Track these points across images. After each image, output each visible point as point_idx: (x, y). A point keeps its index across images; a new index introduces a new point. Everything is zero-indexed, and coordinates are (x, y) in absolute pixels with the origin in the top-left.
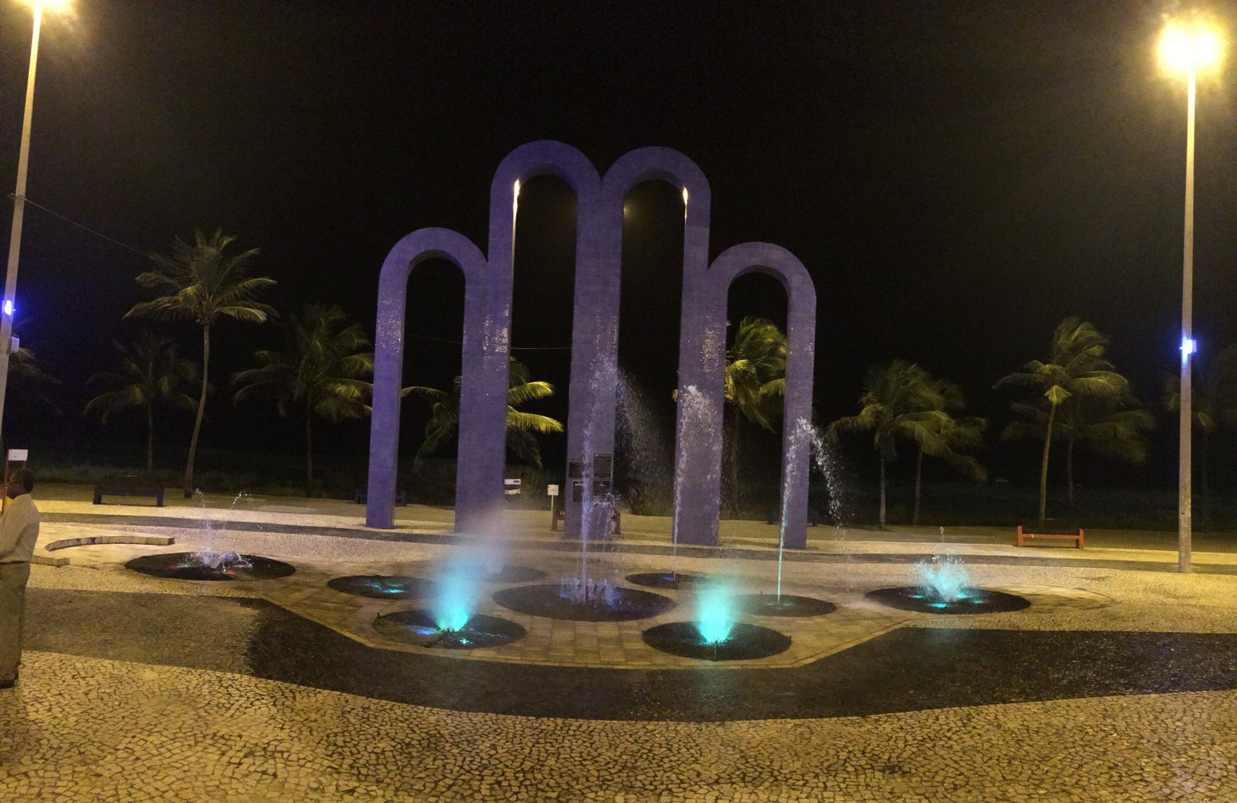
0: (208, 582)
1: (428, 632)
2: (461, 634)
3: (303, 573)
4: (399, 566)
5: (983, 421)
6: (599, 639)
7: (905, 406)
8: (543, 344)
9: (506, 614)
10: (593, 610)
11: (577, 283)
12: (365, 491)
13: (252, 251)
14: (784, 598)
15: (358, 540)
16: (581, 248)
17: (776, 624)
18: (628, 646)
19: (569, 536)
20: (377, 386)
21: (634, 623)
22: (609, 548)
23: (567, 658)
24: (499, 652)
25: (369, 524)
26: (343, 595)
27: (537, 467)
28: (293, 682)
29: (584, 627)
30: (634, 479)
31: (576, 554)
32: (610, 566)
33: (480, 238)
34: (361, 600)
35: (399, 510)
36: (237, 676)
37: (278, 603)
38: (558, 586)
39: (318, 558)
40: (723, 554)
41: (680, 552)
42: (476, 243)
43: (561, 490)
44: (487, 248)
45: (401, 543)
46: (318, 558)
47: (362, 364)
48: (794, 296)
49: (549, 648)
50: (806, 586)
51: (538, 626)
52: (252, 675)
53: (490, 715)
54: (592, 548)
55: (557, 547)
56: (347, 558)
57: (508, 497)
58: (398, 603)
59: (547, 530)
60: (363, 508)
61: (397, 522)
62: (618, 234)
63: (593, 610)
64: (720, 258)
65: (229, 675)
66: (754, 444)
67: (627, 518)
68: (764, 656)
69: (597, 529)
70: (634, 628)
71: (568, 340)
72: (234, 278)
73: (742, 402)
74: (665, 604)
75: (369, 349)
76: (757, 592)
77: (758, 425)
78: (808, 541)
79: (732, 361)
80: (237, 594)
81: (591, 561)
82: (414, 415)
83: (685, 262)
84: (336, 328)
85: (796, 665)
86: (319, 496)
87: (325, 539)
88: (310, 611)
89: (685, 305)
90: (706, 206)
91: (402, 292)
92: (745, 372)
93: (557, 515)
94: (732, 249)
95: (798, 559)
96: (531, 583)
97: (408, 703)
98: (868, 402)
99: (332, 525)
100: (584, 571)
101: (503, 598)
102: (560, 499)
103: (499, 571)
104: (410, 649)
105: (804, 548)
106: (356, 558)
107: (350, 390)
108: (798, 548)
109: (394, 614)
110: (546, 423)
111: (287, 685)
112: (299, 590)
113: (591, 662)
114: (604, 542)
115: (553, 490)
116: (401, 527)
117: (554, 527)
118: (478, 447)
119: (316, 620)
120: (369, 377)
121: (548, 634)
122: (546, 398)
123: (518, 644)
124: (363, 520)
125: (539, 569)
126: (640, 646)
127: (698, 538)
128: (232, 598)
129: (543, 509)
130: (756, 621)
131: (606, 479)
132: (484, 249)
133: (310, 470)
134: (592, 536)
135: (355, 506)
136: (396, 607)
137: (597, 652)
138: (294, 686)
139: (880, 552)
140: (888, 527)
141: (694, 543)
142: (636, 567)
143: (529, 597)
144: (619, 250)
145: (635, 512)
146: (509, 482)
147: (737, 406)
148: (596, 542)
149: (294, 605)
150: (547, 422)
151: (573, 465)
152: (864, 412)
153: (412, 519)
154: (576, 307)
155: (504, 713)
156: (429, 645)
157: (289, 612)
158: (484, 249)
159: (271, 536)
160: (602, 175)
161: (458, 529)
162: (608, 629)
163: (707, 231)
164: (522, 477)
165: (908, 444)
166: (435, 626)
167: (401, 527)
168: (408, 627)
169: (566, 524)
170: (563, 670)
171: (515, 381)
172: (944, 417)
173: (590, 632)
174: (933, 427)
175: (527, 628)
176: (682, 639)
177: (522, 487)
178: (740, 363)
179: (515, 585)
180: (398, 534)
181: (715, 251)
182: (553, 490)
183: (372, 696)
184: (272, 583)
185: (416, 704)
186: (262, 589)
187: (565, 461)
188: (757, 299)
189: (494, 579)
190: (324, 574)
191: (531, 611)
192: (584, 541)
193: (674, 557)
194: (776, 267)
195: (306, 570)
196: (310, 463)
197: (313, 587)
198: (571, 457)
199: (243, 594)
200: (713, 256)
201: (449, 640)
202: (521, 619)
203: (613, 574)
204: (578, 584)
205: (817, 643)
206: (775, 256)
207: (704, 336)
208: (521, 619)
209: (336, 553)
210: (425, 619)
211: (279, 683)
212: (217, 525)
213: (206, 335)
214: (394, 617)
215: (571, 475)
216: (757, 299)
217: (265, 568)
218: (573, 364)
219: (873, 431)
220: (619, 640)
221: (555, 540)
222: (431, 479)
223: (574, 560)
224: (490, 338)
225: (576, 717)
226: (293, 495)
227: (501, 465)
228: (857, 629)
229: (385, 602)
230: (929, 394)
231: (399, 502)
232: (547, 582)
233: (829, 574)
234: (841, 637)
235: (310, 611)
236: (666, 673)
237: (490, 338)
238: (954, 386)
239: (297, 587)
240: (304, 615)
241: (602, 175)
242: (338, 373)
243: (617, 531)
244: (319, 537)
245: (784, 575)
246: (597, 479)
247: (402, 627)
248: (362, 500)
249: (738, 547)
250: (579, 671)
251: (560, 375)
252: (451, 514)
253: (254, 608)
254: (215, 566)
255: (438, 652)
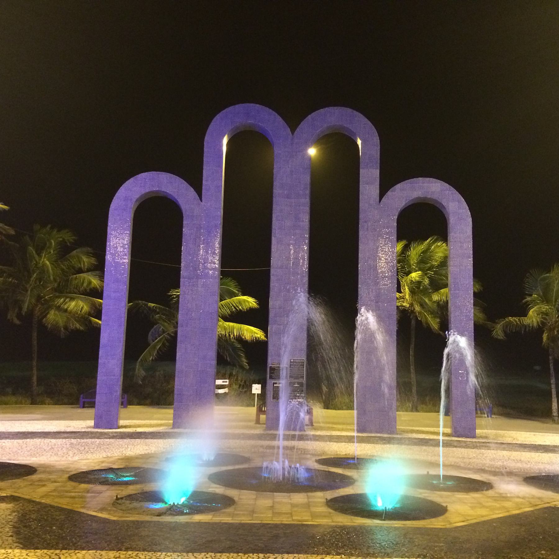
1: (159, 506)
3: (44, 472)
4: (128, 459)
6: (293, 506)
9: (219, 490)
10: (290, 485)
11: (274, 219)
12: (93, 395)
14: (446, 477)
15: (89, 441)
16: (277, 191)
17: (437, 497)
18: (314, 509)
19: (269, 428)
20: (106, 303)
21: (319, 494)
22: (301, 438)
23: (268, 518)
25: (96, 426)
26: (83, 486)
28: (56, 549)
30: (323, 380)
32: (304, 452)
33: (196, 183)
35: (123, 412)
36: (10, 551)
37: (27, 497)
39: (56, 458)
40: (400, 442)
41: (361, 440)
42: (191, 185)
43: (263, 388)
44: (201, 194)
46: (56, 458)
48: (452, 220)
50: (469, 469)
51: (245, 497)
52: (22, 549)
53: (210, 554)
54: (287, 438)
55: (260, 437)
57: (218, 395)
58: (131, 487)
59: (252, 424)
60: (91, 412)
62: (307, 179)
63: (290, 485)
64: (389, 193)
67: (319, 412)
68: (424, 519)
69: (293, 422)
70: (320, 497)
71: (268, 264)
73: (417, 308)
74: (346, 481)
75: (99, 267)
76: (423, 472)
78: (478, 431)
81: (286, 448)
82: (138, 330)
83: (361, 197)
84: (65, 251)
86: (43, 403)
87: (59, 441)
88: (56, 500)
91: (129, 224)
92: (419, 283)
93: (260, 411)
94: (398, 186)
95: (467, 446)
96: (237, 467)
97: (149, 551)
98: (534, 302)
99: (62, 429)
101: (217, 478)
102: (262, 396)
103: (212, 458)
104: (147, 518)
105: (474, 437)
106: (89, 456)
107: (78, 305)
109: (129, 496)
110: (251, 332)
111: (52, 551)
112: (44, 485)
113: (286, 520)
114: (297, 433)
115: (256, 389)
116: (125, 427)
117: (258, 421)
118: (194, 356)
120: (98, 293)
121: (252, 502)
122: (251, 310)
124: (91, 423)
125: (246, 455)
126: (324, 509)
127: (376, 426)
129: (248, 406)
130: (421, 493)
131: (300, 380)
132: (199, 190)
133: (35, 379)
134: (288, 427)
135: (80, 410)
136: (131, 490)
138: (58, 551)
141: (377, 432)
142: (324, 453)
143: (240, 474)
145: (327, 407)
146: (219, 382)
147: (413, 312)
149: (42, 497)
150: (252, 332)
151: (272, 369)
152: (531, 313)
153: (136, 419)
154: (273, 238)
155: (220, 552)
156: (159, 515)
157: (39, 503)
158: (199, 190)
162: (299, 498)
163: (378, 171)
164: (230, 377)
166: (163, 501)
167: (125, 427)
168: (142, 504)
169: (267, 419)
170: (264, 525)
171: (225, 294)
173: (285, 500)
175: (236, 499)
176: (356, 505)
177: (229, 386)
181: (385, 187)
182: (256, 389)
183: (121, 550)
184: (19, 482)
185: (155, 552)
187: (267, 366)
188: (420, 223)
189: (208, 464)
190: (63, 471)
191: (240, 486)
192: (281, 431)
193: (356, 445)
194: (435, 197)
195: (48, 469)
196: (35, 372)
197: (55, 482)
198: (271, 362)
200: (383, 193)
202: (232, 493)
204: (278, 466)
205: (471, 512)
206: (434, 189)
207: (380, 253)
208: (232, 493)
209: (71, 453)
210: (155, 497)
211: (45, 551)
214: (130, 497)
215: (271, 378)
216: (420, 223)
218: (272, 285)
220: (308, 506)
221: (258, 431)
223: (273, 447)
224: (203, 255)
226: (16, 403)
227: (212, 370)
228: (508, 504)
231: (126, 403)
232: (252, 465)
233: (493, 459)
234: (492, 509)
235: (56, 500)
236: (343, 528)
237: (203, 255)
239: (42, 483)
240: (53, 504)
241: (293, 133)
242: (64, 289)
243: (311, 423)
244: (53, 441)
245: (450, 459)
246: (293, 380)
250: (276, 526)
253: (7, 503)
255: (168, 519)
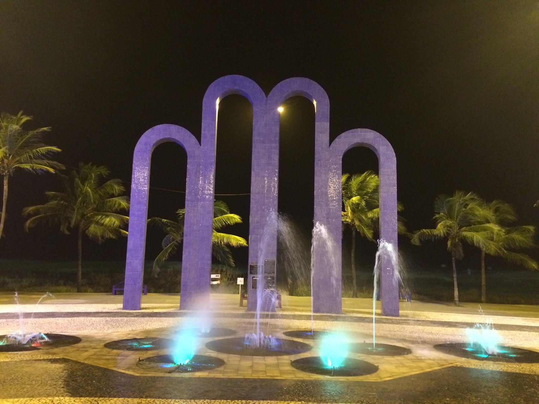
0: (25, 352)
1: (170, 366)
2: (187, 365)
3: (87, 341)
4: (148, 332)
5: (531, 228)
6: (267, 366)
7: (467, 222)
8: (233, 190)
9: (214, 354)
10: (264, 351)
13: (45, 129)
14: (378, 345)
15: (119, 318)
16: (255, 138)
17: (371, 359)
20: (131, 219)
21: (286, 357)
22: (273, 317)
23: (248, 374)
24: (209, 373)
25: (125, 308)
27: (230, 266)
28: (95, 397)
29: (258, 360)
30: (289, 274)
31: (254, 320)
32: (275, 326)
33: (197, 133)
34: (127, 352)
35: (144, 298)
36: (62, 398)
37: (74, 359)
38: (244, 338)
39: (95, 331)
40: (344, 319)
41: (316, 318)
43: (245, 281)
45: (147, 319)
46: (95, 331)
47: (120, 204)
49: (238, 370)
50: (394, 339)
51: (232, 359)
53: (207, 400)
54: (262, 316)
55: (243, 316)
56: (113, 330)
57: (212, 286)
58: (150, 352)
59: (237, 306)
60: (121, 298)
61: (143, 305)
63: (264, 351)
65: (57, 398)
66: (358, 248)
68: (362, 375)
69: (267, 305)
70: (286, 359)
72: (28, 145)
75: (127, 193)
76: (361, 341)
77: (365, 237)
78: (401, 312)
79: (350, 198)
80: (46, 357)
81: (262, 324)
82: (154, 238)
84: (101, 181)
85: (379, 380)
87: (98, 319)
89: (316, 169)
90: (327, 110)
91: (148, 162)
92: (358, 204)
93: (243, 297)
95: (393, 323)
97: (163, 398)
98: (441, 219)
99: (100, 310)
100: (258, 329)
101: (212, 346)
102: (245, 286)
103: (208, 331)
104: (161, 375)
107: (112, 221)
108: (395, 316)
110: (236, 240)
111: (92, 398)
112: (87, 351)
113: (262, 376)
114: (270, 313)
115: (240, 281)
116: (146, 308)
117: (241, 304)
119: (101, 366)
120: (126, 212)
122: (237, 224)
123: (221, 369)
124: (121, 306)
125: (233, 329)
126: (289, 368)
127: (328, 308)
128: (44, 360)
129: (234, 293)
130: (359, 357)
131: (272, 275)
134: (263, 309)
136: (150, 354)
137: (265, 371)
138: (96, 399)
139: (451, 320)
140: (461, 304)
141: (328, 312)
142: (289, 327)
143: (228, 343)
144: (278, 139)
145: (291, 294)
146: (213, 276)
147: (354, 225)
148: (266, 313)
149: (85, 359)
150: (237, 240)
152: (439, 226)
153: (154, 303)
154: (252, 172)
156: (170, 372)
157: (83, 364)
159: (60, 320)
160: (267, 95)
161: (182, 306)
162: (271, 360)
163: (329, 124)
165: (471, 249)
166: (172, 362)
167: (146, 308)
168: (158, 364)
169: (248, 303)
170: (246, 380)
172: (496, 228)
174: (488, 233)
175: (226, 361)
176: (312, 365)
177: (221, 279)
178: (355, 199)
179: (217, 339)
180: (145, 313)
182: (240, 281)
183: (142, 398)
184: (68, 348)
185: (167, 399)
186: (60, 352)
188: (360, 161)
189: (206, 335)
190: (100, 341)
192: (258, 312)
193: (313, 321)
194: (370, 142)
195: (89, 339)
197: (95, 348)
198: (251, 262)
199: (51, 357)
201: (181, 369)
202: (223, 356)
203: (277, 332)
204: (256, 337)
205: (396, 370)
207: (330, 183)
208: (223, 356)
209: (106, 327)
210: (167, 359)
211: (88, 398)
212: (27, 315)
213: (6, 182)
214: (149, 359)
215: (251, 273)
216: (360, 161)
217: (57, 340)
218: (251, 206)
219: (445, 239)
220: (277, 366)
221: (241, 312)
222: (165, 277)
223: (252, 323)
224: (202, 184)
225: (252, 400)
227: (209, 268)
228: (422, 365)
229: (143, 352)
230: (482, 212)
232: (238, 336)
233: (412, 332)
234: (411, 368)
235: (96, 361)
236: (303, 381)
237: (202, 184)
238: (506, 205)
240: (93, 364)
241: (267, 95)
242: (102, 208)
243: (280, 306)
244: (93, 319)
246: (267, 275)
247: (153, 364)
248: (121, 293)
249: (352, 315)
250: (255, 380)
251: (244, 209)
252: (177, 298)
253: (60, 364)
254: (25, 342)
255: (176, 375)
